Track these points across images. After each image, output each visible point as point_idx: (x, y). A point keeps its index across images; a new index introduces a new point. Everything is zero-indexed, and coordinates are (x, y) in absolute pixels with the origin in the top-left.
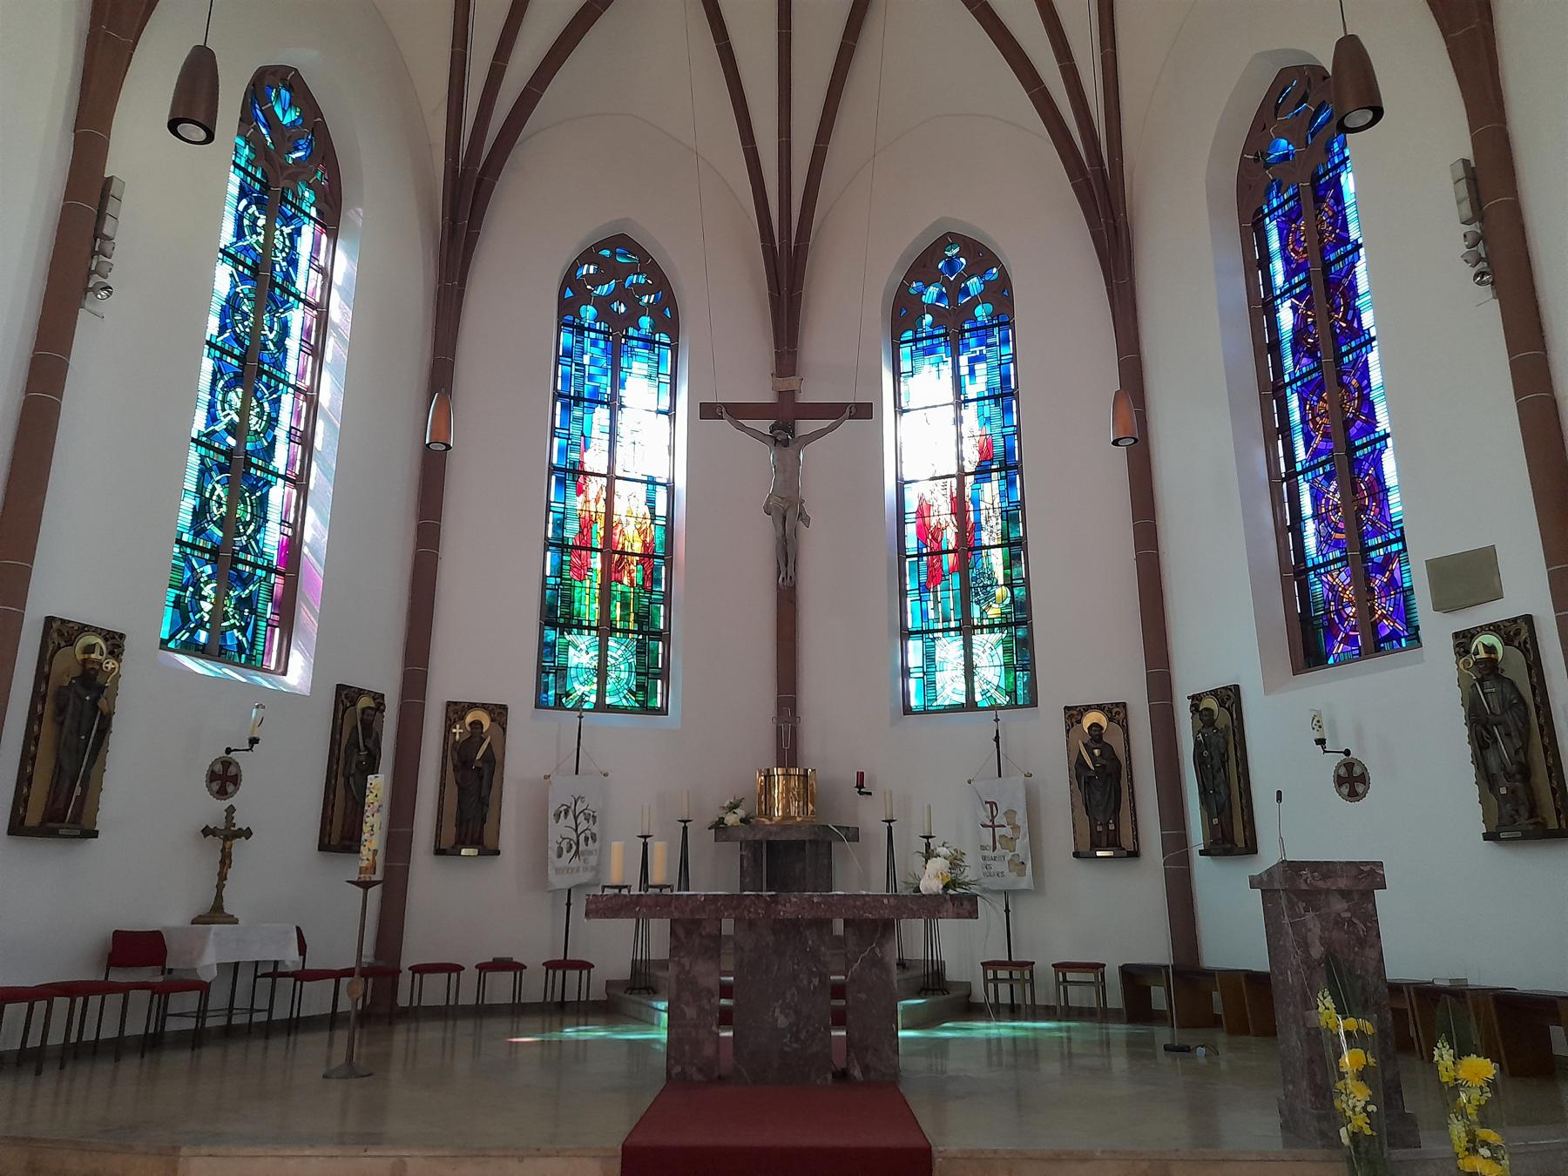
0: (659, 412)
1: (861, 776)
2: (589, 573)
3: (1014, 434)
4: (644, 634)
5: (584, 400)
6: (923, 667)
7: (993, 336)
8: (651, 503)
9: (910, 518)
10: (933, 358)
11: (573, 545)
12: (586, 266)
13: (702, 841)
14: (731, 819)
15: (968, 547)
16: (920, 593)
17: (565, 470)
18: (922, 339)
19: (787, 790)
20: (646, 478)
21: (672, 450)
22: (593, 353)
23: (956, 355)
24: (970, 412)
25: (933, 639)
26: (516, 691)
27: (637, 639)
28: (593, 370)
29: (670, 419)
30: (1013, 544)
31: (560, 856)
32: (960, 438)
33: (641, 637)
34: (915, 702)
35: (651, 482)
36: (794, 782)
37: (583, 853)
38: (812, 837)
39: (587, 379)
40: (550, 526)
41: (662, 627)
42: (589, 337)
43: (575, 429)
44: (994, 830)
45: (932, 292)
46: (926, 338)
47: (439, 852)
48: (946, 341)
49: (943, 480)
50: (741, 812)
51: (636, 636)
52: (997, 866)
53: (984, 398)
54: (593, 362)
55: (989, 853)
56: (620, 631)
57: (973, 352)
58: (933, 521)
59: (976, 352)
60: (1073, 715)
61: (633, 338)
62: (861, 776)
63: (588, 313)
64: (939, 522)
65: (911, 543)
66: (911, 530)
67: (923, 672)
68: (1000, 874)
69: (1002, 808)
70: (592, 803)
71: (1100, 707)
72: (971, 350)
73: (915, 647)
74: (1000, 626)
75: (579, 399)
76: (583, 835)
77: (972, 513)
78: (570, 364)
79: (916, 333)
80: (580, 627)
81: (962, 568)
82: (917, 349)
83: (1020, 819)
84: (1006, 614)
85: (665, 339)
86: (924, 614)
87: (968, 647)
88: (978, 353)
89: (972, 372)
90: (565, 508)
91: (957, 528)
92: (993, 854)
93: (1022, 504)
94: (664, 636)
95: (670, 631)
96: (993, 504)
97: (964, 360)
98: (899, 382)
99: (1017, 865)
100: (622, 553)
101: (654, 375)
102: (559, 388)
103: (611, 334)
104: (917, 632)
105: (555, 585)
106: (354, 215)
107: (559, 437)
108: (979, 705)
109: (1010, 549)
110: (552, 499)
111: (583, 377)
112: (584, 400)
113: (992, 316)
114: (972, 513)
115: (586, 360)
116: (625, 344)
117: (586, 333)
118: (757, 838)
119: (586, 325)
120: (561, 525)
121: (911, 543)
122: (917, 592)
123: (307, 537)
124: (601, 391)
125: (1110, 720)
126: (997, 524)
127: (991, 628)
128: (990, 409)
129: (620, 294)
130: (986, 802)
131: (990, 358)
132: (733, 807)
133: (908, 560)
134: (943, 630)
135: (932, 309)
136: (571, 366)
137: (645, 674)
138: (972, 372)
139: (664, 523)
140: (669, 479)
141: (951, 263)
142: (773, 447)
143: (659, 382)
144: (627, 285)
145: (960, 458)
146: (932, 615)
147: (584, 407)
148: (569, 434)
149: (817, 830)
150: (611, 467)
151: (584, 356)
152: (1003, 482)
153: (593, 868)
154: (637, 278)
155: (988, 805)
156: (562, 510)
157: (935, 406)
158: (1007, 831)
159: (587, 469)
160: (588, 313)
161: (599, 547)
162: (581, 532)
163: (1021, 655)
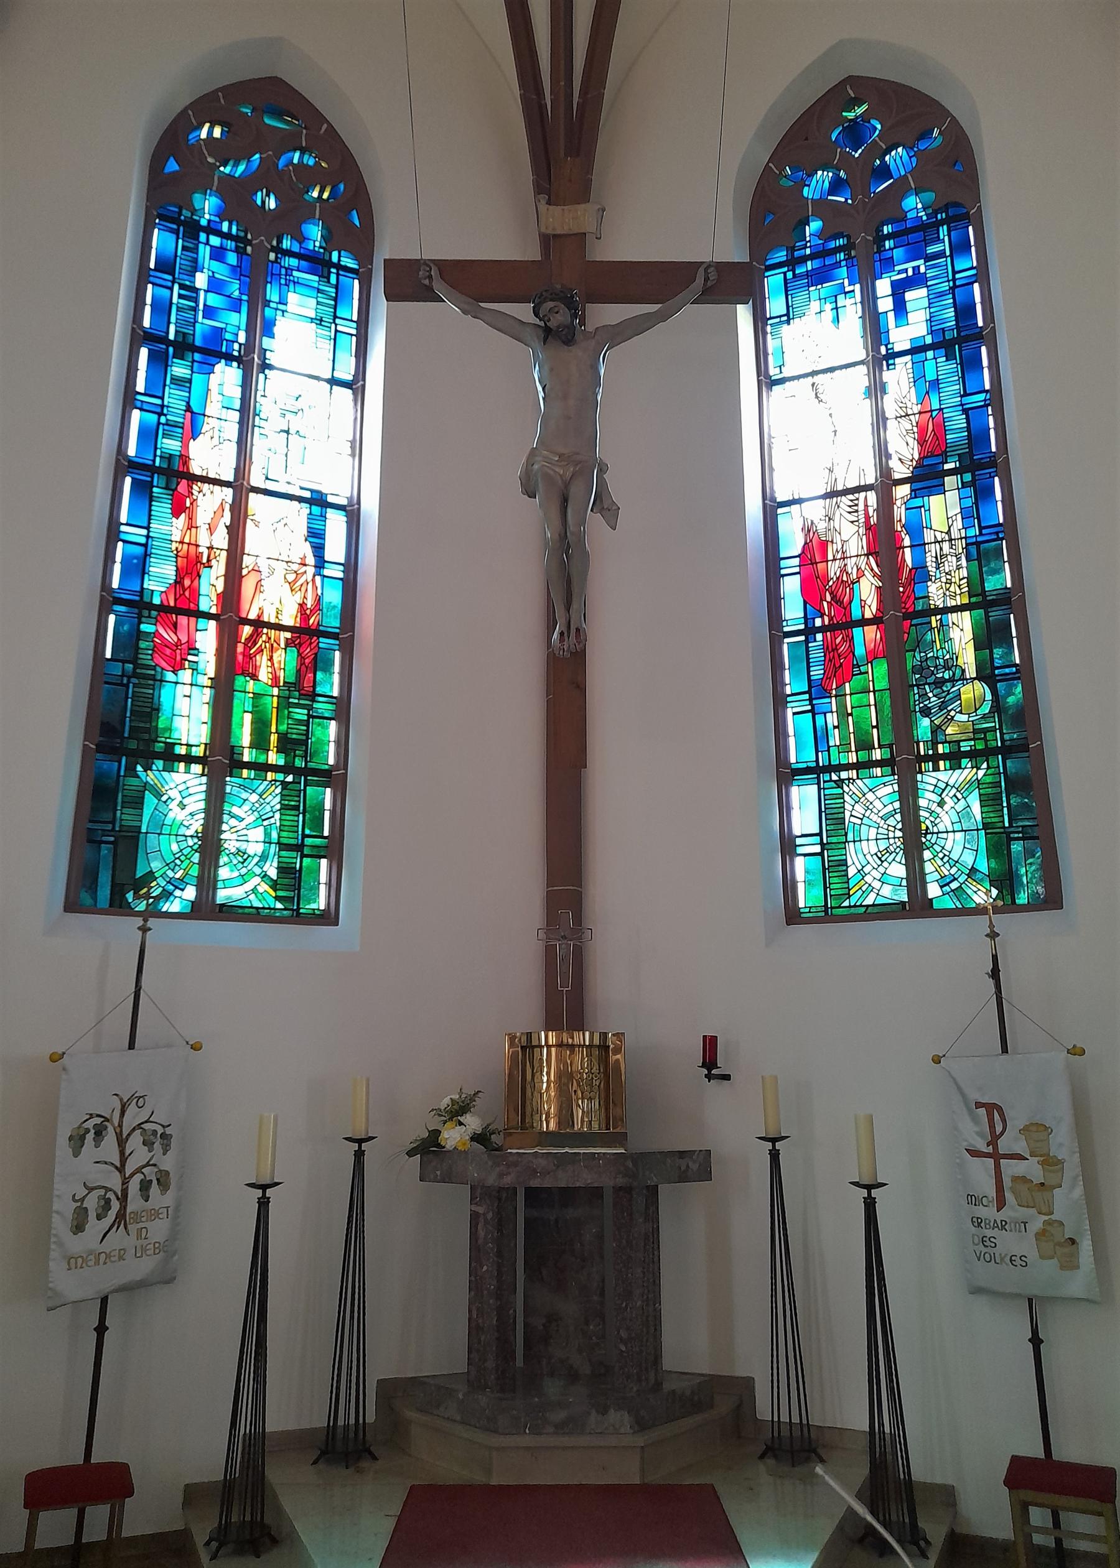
0: (333, 382)
1: (710, 1044)
2: (190, 658)
3: (987, 406)
4: (298, 772)
5: (195, 349)
6: (820, 834)
7: (938, 240)
9: (790, 565)
10: (827, 288)
11: (162, 604)
12: (207, 125)
14: (453, 1137)
16: (811, 700)
17: (151, 469)
18: (804, 260)
19: (565, 1078)
20: (307, 494)
21: (357, 448)
25: (840, 783)
27: (284, 784)
28: (214, 300)
29: (355, 394)
30: (993, 603)
31: (78, 1227)
32: (880, 420)
33: (290, 778)
34: (808, 897)
35: (318, 501)
36: (580, 1062)
37: (137, 1217)
38: (621, 1181)
39: (201, 314)
40: (117, 568)
41: (331, 761)
42: (207, 243)
43: (174, 398)
44: (997, 1166)
46: (812, 257)
48: (848, 258)
49: (851, 497)
50: (473, 1122)
51: (280, 776)
52: (1009, 1243)
53: (924, 348)
54: (215, 286)
55: (988, 1212)
56: (249, 766)
57: (900, 272)
58: (833, 569)
59: (906, 270)
61: (289, 253)
62: (710, 1044)
63: (208, 206)
64: (844, 570)
65: (793, 609)
66: (791, 587)
67: (821, 843)
68: (1015, 1261)
69: (1017, 1119)
72: (897, 268)
74: (972, 755)
75: (184, 347)
76: (138, 1177)
77: (908, 551)
78: (169, 284)
79: (791, 249)
82: (794, 275)
83: (1061, 1145)
84: (985, 731)
85: (349, 262)
87: (908, 795)
88: (910, 273)
89: (900, 307)
90: (148, 537)
91: (880, 578)
92: (1000, 1216)
93: (1009, 530)
95: (346, 768)
96: (948, 533)
97: (883, 286)
98: (765, 334)
99: (1059, 1244)
101: (328, 319)
102: (147, 323)
103: (249, 242)
104: (807, 771)
105: (123, 676)
107: (141, 409)
108: (936, 905)
109: (986, 613)
110: (123, 518)
111: (195, 309)
112: (195, 349)
113: (932, 210)
114: (908, 551)
115: (201, 280)
116: (276, 261)
117: (203, 237)
118: (508, 1180)
119: (204, 222)
120: (138, 567)
121: (793, 609)
122: (807, 696)
124: (228, 336)
126: (959, 568)
127: (955, 759)
128: (938, 366)
129: (265, 178)
130: (979, 1105)
131: (934, 278)
132: (457, 1111)
133: (786, 640)
134: (858, 766)
135: (822, 207)
136: (171, 289)
137: (299, 848)
138: (900, 307)
139: (341, 575)
140: (350, 499)
141: (855, 132)
142: (538, 345)
143: (336, 331)
144: (282, 163)
145: (882, 452)
146: (835, 739)
147: (193, 361)
148: (162, 406)
149: (630, 1164)
151: (198, 274)
152: (969, 491)
153: (160, 1248)
154: (301, 158)
155: (982, 1111)
156: (143, 540)
157: (831, 370)
158: (1031, 1168)
159: (196, 469)
161: (214, 611)
162: (179, 582)
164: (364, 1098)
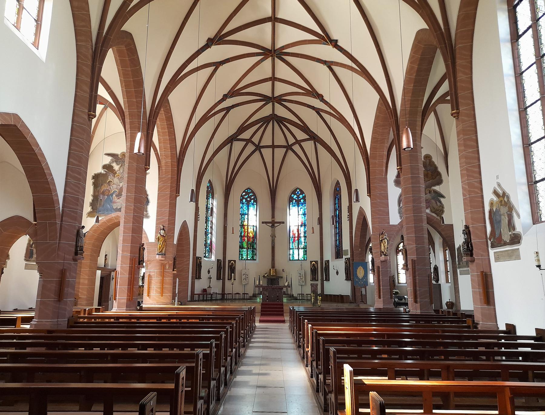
8: (253, 229)
13: (262, 278)
14: (265, 275)
15: (299, 237)
21: (256, 221)
22: (245, 207)
23: (298, 207)
24: (300, 216)
26: (237, 259)
34: (291, 259)
35: (253, 226)
36: (274, 271)
45: (295, 196)
47: (228, 279)
50: (267, 274)
52: (301, 282)
60: (311, 262)
63: (244, 200)
69: (301, 274)
70: (247, 273)
71: (314, 261)
73: (291, 251)
74: (303, 248)
75: (243, 214)
80: (244, 248)
81: (298, 240)
86: (293, 246)
87: (298, 251)
94: (256, 249)
100: (250, 237)
106: (216, 196)
115: (244, 208)
123: (213, 241)
125: (315, 263)
127: (302, 249)
129: (249, 197)
132: (266, 274)
138: (300, 210)
150: (248, 224)
158: (302, 277)
160: (244, 200)
163: (305, 253)
164: (381, 283)
